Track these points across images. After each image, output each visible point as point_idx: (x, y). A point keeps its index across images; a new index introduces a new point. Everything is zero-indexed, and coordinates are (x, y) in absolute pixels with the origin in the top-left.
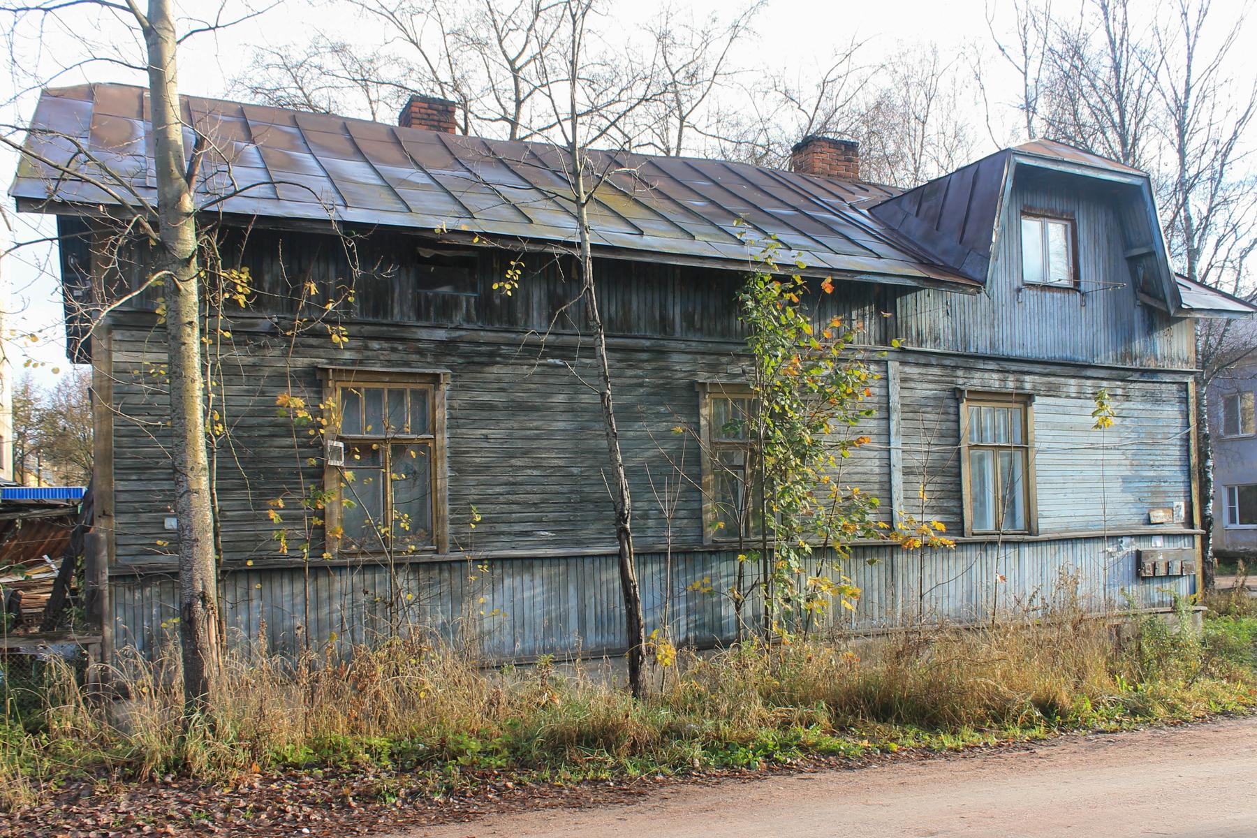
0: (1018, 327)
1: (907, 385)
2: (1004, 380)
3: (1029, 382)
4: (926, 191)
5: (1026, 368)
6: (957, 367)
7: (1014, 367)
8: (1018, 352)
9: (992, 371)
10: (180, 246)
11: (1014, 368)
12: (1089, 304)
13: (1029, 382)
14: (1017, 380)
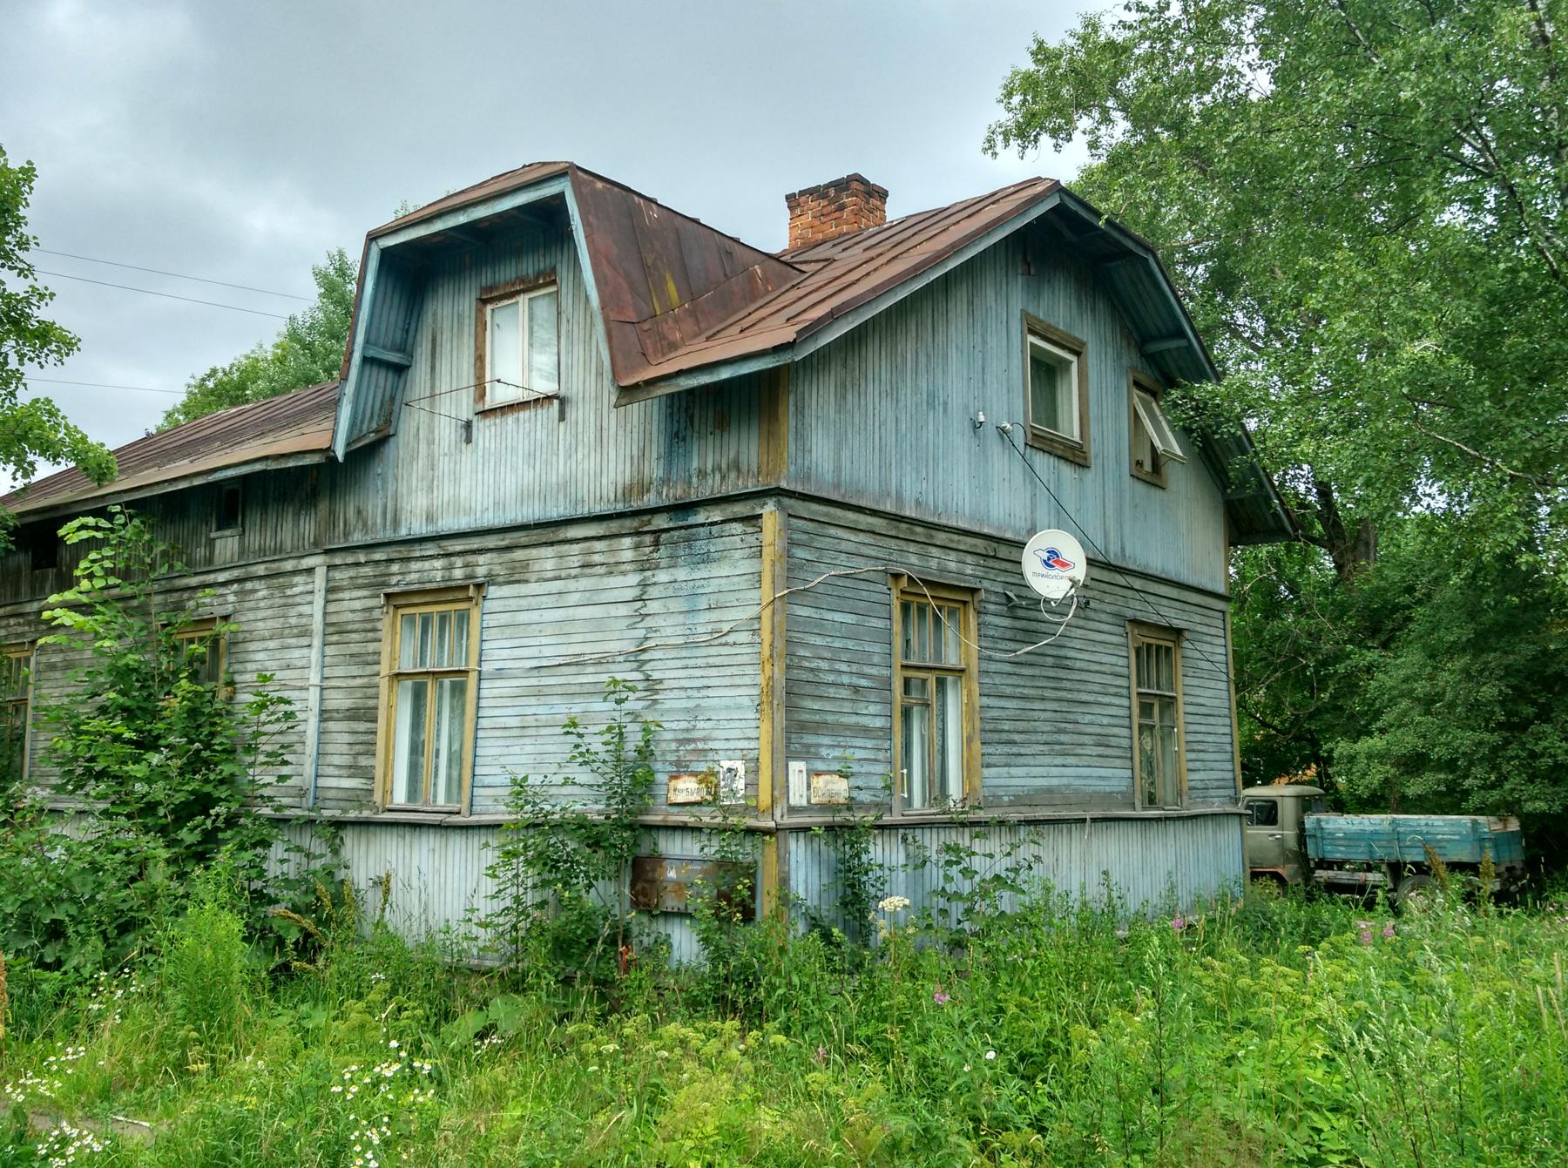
0: (466, 483)
1: (335, 596)
2: (450, 568)
3: (483, 565)
4: (612, 316)
5: (476, 543)
6: (390, 561)
7: (458, 546)
8: (464, 524)
9: (432, 557)
10: (990, 293)
11: (458, 548)
12: (571, 413)
13: (483, 565)
14: (466, 566)
